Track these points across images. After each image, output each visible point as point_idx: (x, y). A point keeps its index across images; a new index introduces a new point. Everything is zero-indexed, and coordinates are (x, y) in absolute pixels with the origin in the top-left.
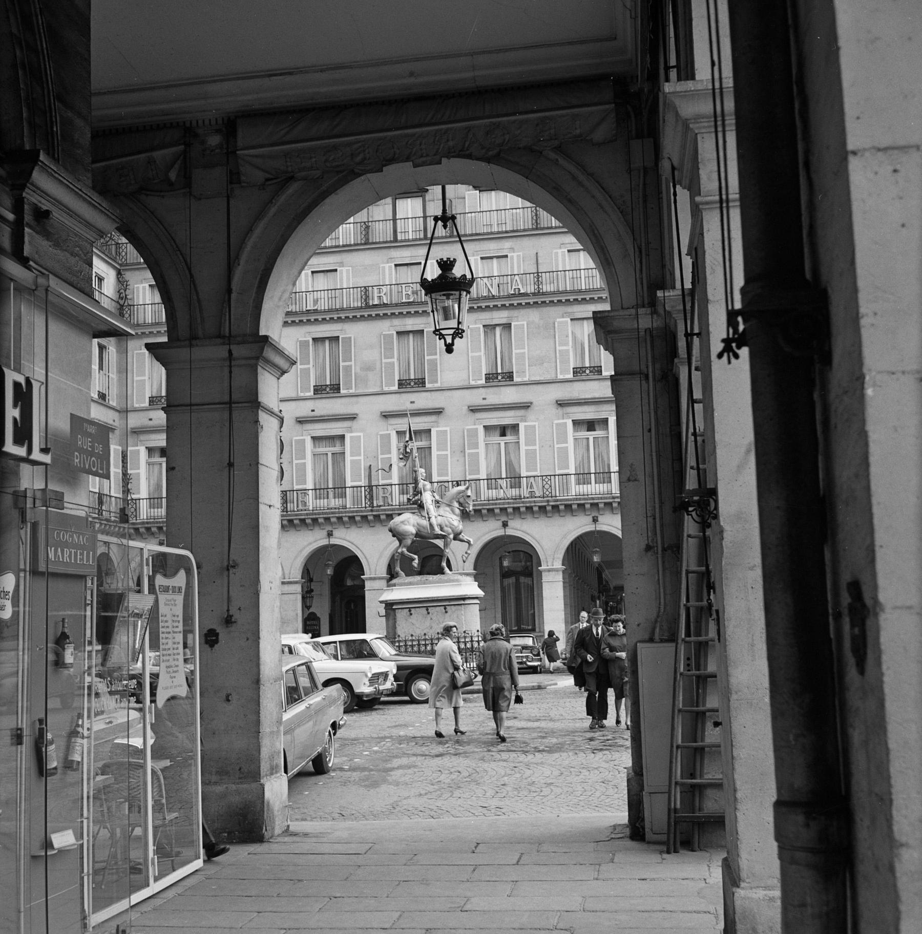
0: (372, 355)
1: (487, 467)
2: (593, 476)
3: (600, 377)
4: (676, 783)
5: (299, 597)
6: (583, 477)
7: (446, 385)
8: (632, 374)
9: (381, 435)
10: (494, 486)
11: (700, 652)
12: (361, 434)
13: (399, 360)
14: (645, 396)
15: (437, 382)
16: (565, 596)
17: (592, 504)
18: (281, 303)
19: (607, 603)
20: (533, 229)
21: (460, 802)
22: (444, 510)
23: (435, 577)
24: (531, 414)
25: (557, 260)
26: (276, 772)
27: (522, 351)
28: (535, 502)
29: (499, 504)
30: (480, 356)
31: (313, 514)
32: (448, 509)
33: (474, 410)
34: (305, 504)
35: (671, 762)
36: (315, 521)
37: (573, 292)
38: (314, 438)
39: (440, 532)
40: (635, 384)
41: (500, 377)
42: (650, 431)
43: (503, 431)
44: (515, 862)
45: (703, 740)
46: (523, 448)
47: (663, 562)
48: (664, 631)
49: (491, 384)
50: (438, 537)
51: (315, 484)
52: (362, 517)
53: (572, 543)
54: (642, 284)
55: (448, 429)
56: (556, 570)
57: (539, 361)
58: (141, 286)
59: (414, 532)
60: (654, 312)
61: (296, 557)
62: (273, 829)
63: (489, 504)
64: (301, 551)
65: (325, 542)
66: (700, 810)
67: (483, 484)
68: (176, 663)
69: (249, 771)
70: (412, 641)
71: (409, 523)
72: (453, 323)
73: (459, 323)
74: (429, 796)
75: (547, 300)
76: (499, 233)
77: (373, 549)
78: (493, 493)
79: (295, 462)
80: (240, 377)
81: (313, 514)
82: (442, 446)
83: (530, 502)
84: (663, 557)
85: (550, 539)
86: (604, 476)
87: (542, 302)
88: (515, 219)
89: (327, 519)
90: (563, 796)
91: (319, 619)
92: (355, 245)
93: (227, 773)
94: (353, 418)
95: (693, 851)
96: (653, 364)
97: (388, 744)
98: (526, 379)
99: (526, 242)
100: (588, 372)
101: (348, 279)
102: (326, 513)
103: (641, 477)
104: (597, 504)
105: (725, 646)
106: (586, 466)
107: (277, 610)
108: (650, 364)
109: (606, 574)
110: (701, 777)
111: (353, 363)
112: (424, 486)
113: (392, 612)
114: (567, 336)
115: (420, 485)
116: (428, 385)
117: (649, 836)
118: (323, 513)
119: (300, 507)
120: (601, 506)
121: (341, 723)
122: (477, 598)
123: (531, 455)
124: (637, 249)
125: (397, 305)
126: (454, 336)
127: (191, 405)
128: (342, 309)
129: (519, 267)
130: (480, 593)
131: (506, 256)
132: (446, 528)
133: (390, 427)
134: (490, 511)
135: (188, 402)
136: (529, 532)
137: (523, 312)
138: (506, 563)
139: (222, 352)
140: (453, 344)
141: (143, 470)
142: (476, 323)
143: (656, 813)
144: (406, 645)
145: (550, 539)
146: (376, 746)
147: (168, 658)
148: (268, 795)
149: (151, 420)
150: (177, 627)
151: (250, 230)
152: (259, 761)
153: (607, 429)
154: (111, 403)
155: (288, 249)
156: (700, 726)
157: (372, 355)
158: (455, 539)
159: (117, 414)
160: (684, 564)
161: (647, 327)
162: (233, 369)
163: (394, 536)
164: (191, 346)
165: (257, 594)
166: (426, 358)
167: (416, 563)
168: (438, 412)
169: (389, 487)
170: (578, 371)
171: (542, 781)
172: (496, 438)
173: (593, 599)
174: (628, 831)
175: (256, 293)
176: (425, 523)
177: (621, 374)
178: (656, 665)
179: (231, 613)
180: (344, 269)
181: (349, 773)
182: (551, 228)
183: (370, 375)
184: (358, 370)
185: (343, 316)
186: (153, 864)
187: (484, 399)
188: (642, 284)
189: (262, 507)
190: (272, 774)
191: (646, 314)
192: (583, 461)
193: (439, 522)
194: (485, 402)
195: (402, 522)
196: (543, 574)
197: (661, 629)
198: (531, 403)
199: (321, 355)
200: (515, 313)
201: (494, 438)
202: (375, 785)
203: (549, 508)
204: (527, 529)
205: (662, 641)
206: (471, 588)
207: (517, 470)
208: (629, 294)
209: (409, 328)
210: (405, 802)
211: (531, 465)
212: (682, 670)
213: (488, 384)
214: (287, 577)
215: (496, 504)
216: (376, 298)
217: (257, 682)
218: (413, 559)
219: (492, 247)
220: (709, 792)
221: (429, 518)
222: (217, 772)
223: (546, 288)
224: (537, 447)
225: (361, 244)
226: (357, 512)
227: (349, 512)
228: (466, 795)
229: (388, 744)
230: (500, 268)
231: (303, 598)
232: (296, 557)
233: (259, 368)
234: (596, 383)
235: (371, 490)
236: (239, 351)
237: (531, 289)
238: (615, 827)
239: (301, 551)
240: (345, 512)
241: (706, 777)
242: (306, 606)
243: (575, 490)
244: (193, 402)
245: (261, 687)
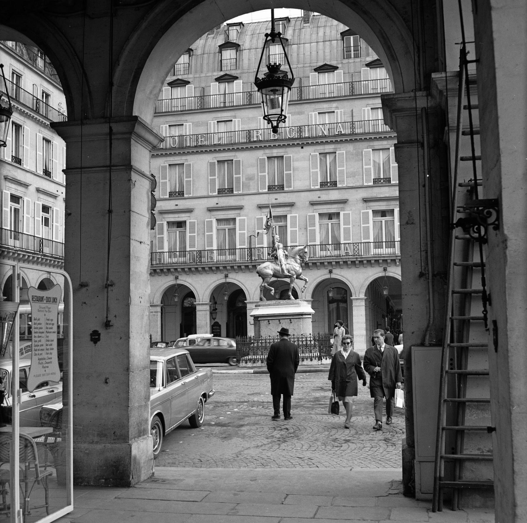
0: (252, 171)
1: (320, 238)
2: (384, 243)
3: (389, 184)
4: (441, 457)
5: (208, 313)
6: (378, 244)
7: (296, 189)
8: (411, 142)
9: (257, 218)
10: (324, 249)
11: (461, 355)
12: (246, 218)
13: (268, 173)
14: (421, 159)
15: (291, 187)
16: (366, 314)
17: (383, 260)
18: (152, 96)
19: (392, 320)
20: (350, 96)
21: (284, 453)
22: (291, 261)
23: (284, 301)
24: (347, 207)
25: (364, 114)
26: (144, 435)
27: (343, 168)
28: (349, 258)
29: (328, 259)
30: (317, 172)
31: (216, 264)
32: (293, 260)
33: (313, 204)
34: (212, 258)
35: (437, 441)
36: (218, 268)
37: (374, 133)
38: (218, 220)
39: (288, 274)
40: (414, 150)
41: (329, 184)
42: (424, 186)
43: (330, 216)
44: (312, 516)
45: (463, 424)
46: (342, 226)
47: (433, 286)
48: (433, 337)
50: (286, 277)
52: (246, 266)
53: (371, 283)
54: (419, 74)
55: (297, 215)
56: (361, 299)
57: (352, 175)
59: (272, 273)
60: (429, 94)
61: (207, 289)
62: (139, 476)
63: (321, 260)
64: (209, 286)
65: (223, 281)
66: (460, 478)
67: (318, 248)
68: (50, 356)
69: (121, 435)
70: (270, 339)
71: (269, 268)
72: (278, 111)
73: (282, 110)
74: (263, 448)
75: (358, 138)
76: (329, 98)
77: (250, 285)
78: (324, 253)
79: (206, 234)
80: (118, 147)
81: (216, 264)
82: (293, 225)
83: (346, 258)
84: (433, 282)
85: (358, 281)
86: (391, 243)
87: (355, 139)
88: (339, 89)
89: (225, 267)
90: (356, 451)
91: (220, 326)
92: (243, 105)
93: (105, 435)
94: (241, 208)
95: (453, 510)
96: (428, 135)
97: (244, 406)
98: (344, 185)
99: (346, 104)
100: (382, 181)
101: (239, 126)
102: (224, 264)
103: (417, 221)
104: (386, 260)
105: (506, 358)
106: (380, 237)
107: (146, 318)
108: (425, 135)
109: (392, 303)
110: (461, 452)
111: (241, 176)
112: (278, 246)
113: (258, 322)
114: (370, 160)
115: (276, 245)
116: (285, 189)
117: (418, 495)
118: (222, 264)
119: (209, 260)
120: (389, 261)
121: (211, 394)
122: (310, 314)
123: (347, 231)
124: (416, 47)
125: (267, 141)
126: (278, 121)
127: (81, 168)
128: (235, 144)
129: (341, 118)
130: (313, 311)
131: (334, 112)
132: (291, 272)
133: (262, 214)
134: (322, 263)
135: (79, 166)
136: (345, 276)
137: (343, 145)
138: (331, 295)
139: (105, 128)
140: (277, 126)
142: (315, 152)
143: (424, 477)
144: (266, 342)
145: (358, 281)
146: (237, 408)
147: (40, 352)
148: (134, 452)
150: (52, 328)
151: (128, 39)
152: (128, 427)
153: (393, 215)
154: (25, 166)
155: (154, 54)
156: (461, 413)
157: (252, 171)
158: (297, 278)
160: (451, 286)
161: (423, 106)
162: (113, 141)
163: (259, 276)
164: (82, 124)
165: (128, 305)
166: (285, 172)
167: (273, 293)
168: (291, 205)
169: (262, 249)
171: (343, 438)
172: (326, 221)
173: (384, 317)
174: (401, 488)
175: (131, 86)
176: (278, 268)
177: (403, 143)
178: (427, 364)
179: (109, 319)
180: (236, 120)
181: (214, 428)
182: (361, 95)
183: (252, 183)
184: (244, 180)
185: (235, 147)
186: (19, 515)
187: (319, 197)
188: (419, 74)
189: (133, 244)
190: (140, 436)
191: (422, 96)
192: (378, 236)
193: (287, 267)
194: (319, 199)
195: (265, 268)
196: (353, 301)
197: (430, 336)
198: (348, 200)
199: (222, 172)
200: (338, 146)
201: (326, 221)
202: (227, 437)
203: (357, 262)
204: (343, 275)
205: (431, 345)
206: (306, 308)
207: (339, 240)
208: (409, 79)
209: (275, 155)
210: (246, 452)
211: (347, 237)
212: (447, 369)
213: (322, 189)
214: (201, 300)
215: (325, 259)
216: (255, 137)
217: (128, 369)
218: (272, 290)
219: (325, 107)
220: (467, 465)
221: (281, 265)
222: (98, 434)
223: (358, 131)
224: (351, 226)
225: (247, 105)
226: (242, 263)
227: (237, 263)
228: (289, 448)
229: (245, 407)
230: (329, 119)
231: (211, 313)
232: (207, 289)
233: (133, 142)
234: (387, 188)
235: (251, 251)
236: (117, 128)
237: (348, 131)
238: (392, 482)
239: (209, 286)
240: (236, 263)
241: (465, 452)
242: (212, 317)
243: (373, 251)
244: (83, 166)
245: (131, 373)
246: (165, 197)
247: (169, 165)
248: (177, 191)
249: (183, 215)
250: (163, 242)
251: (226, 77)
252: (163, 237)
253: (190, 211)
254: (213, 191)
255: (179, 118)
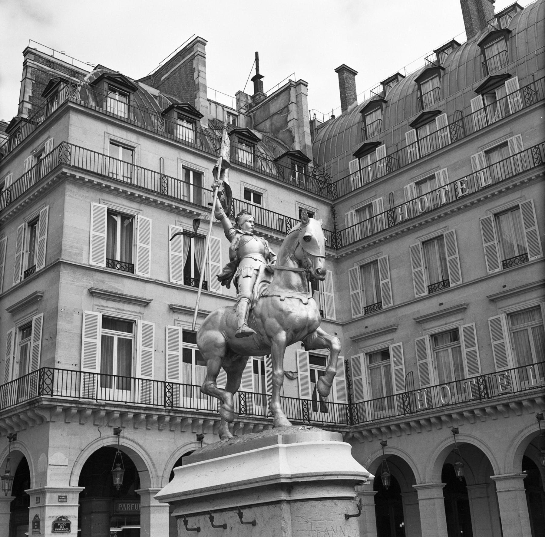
38: (511, 315)
46: (464, 351)
49: (435, 293)
51: (519, 363)
58: (476, 155)
65: (450, 442)
79: (493, 344)
141: (364, 376)
149: (366, 327)
159: (340, 327)
170: (431, 289)
196: (30, 510)
214: (502, 471)
246: (422, 295)
247: (423, 243)
248: (441, 280)
249: (453, 319)
250: (427, 371)
251: (368, 147)
252: (361, 379)
253: (392, 329)
254: (421, 290)
255: (427, 167)
